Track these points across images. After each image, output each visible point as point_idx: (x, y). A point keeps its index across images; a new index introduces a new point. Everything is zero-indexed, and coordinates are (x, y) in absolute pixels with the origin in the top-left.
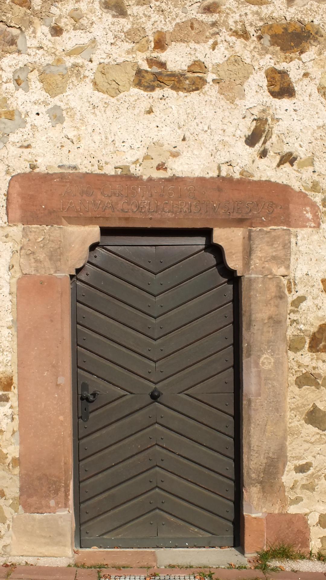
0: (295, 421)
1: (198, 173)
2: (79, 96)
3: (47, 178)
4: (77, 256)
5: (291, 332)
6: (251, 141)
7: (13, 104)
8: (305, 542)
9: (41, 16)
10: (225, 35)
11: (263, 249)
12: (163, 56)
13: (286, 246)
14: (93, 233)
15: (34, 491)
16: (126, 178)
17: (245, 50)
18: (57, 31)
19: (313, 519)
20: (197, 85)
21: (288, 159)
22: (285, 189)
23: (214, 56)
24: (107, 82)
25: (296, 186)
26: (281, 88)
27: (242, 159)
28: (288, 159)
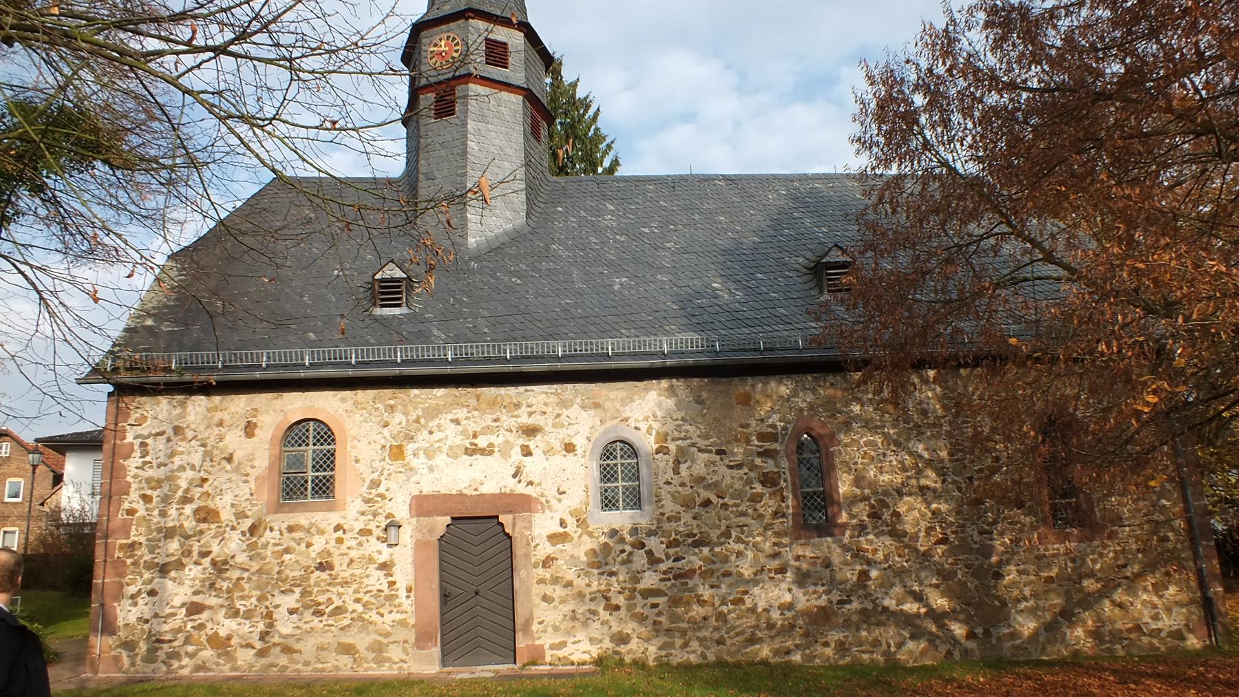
0: (537, 600)
1: (491, 492)
2: (441, 460)
3: (427, 496)
4: (441, 530)
5: (533, 560)
6: (514, 476)
7: (412, 465)
8: (544, 658)
9: (424, 427)
10: (502, 431)
11: (519, 525)
12: (476, 441)
13: (530, 522)
14: (448, 520)
15: (422, 640)
16: (461, 495)
17: (511, 437)
18: (431, 433)
19: (547, 647)
20: (491, 453)
21: (531, 483)
22: (529, 496)
23: (497, 440)
24: (452, 454)
25: (534, 495)
26: (527, 452)
27: (511, 485)
28: (531, 483)
